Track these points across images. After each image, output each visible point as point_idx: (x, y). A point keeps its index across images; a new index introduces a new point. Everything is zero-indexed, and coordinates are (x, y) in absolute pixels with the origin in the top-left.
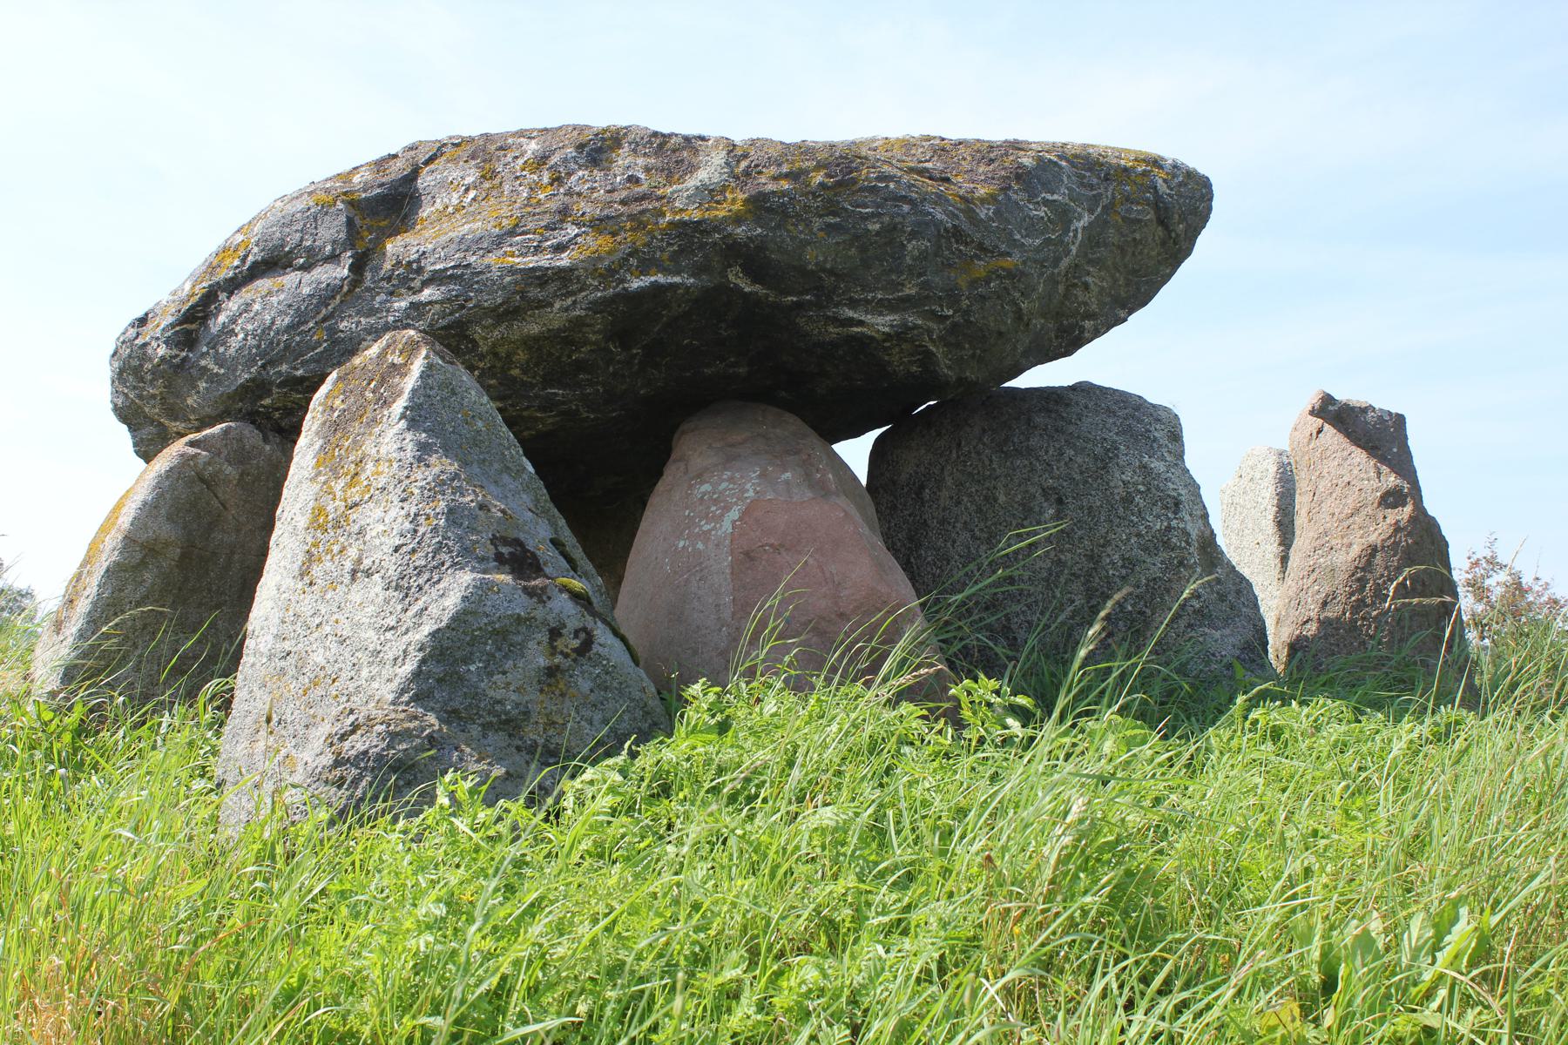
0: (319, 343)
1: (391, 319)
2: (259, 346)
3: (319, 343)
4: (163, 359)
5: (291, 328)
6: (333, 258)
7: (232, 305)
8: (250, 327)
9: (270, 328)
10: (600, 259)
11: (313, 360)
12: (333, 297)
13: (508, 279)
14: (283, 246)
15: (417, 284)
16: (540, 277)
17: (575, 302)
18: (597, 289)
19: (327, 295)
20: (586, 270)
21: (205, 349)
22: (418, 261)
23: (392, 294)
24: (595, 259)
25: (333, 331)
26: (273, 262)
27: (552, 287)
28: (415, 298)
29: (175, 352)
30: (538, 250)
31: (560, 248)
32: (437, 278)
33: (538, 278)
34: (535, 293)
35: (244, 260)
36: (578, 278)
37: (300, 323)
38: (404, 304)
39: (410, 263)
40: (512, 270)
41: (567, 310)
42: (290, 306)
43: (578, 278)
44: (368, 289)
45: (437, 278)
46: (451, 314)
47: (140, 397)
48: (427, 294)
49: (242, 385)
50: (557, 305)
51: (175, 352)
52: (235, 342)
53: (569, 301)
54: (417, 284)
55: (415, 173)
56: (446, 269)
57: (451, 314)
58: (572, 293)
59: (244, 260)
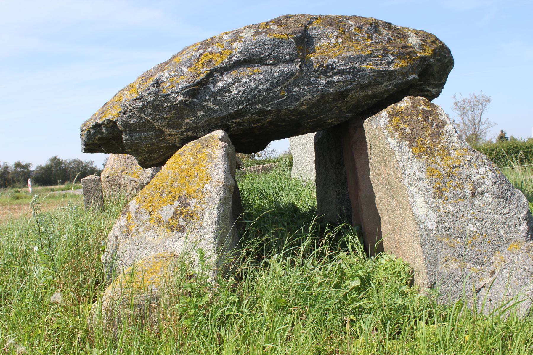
0: (283, 96)
1: (319, 87)
2: (246, 97)
3: (283, 96)
4: (181, 102)
5: (267, 90)
6: (290, 61)
7: (228, 78)
8: (242, 89)
9: (255, 90)
10: (404, 68)
11: (277, 103)
12: (291, 78)
13: (372, 74)
14: (260, 55)
15: (330, 74)
16: (382, 74)
17: (390, 84)
18: (400, 79)
19: (285, 77)
20: (399, 72)
21: (208, 98)
22: (332, 65)
23: (317, 77)
24: (402, 68)
25: (289, 91)
26: (249, 61)
27: (386, 78)
28: (330, 79)
29: (188, 98)
30: (381, 64)
31: (389, 63)
32: (341, 72)
33: (382, 74)
34: (380, 80)
35: (230, 59)
36: (395, 75)
37: (273, 88)
38: (324, 82)
39: (328, 66)
40: (374, 71)
41: (387, 86)
42: (267, 80)
43: (395, 75)
44: (306, 75)
45: (341, 72)
46: (345, 86)
47: (154, 119)
48: (336, 78)
49: (230, 114)
50: (384, 85)
51: (188, 98)
52: (228, 96)
53: (389, 83)
54: (330, 74)
55: (306, 29)
56: (346, 69)
57: (345, 86)
58: (391, 80)
59: (230, 59)
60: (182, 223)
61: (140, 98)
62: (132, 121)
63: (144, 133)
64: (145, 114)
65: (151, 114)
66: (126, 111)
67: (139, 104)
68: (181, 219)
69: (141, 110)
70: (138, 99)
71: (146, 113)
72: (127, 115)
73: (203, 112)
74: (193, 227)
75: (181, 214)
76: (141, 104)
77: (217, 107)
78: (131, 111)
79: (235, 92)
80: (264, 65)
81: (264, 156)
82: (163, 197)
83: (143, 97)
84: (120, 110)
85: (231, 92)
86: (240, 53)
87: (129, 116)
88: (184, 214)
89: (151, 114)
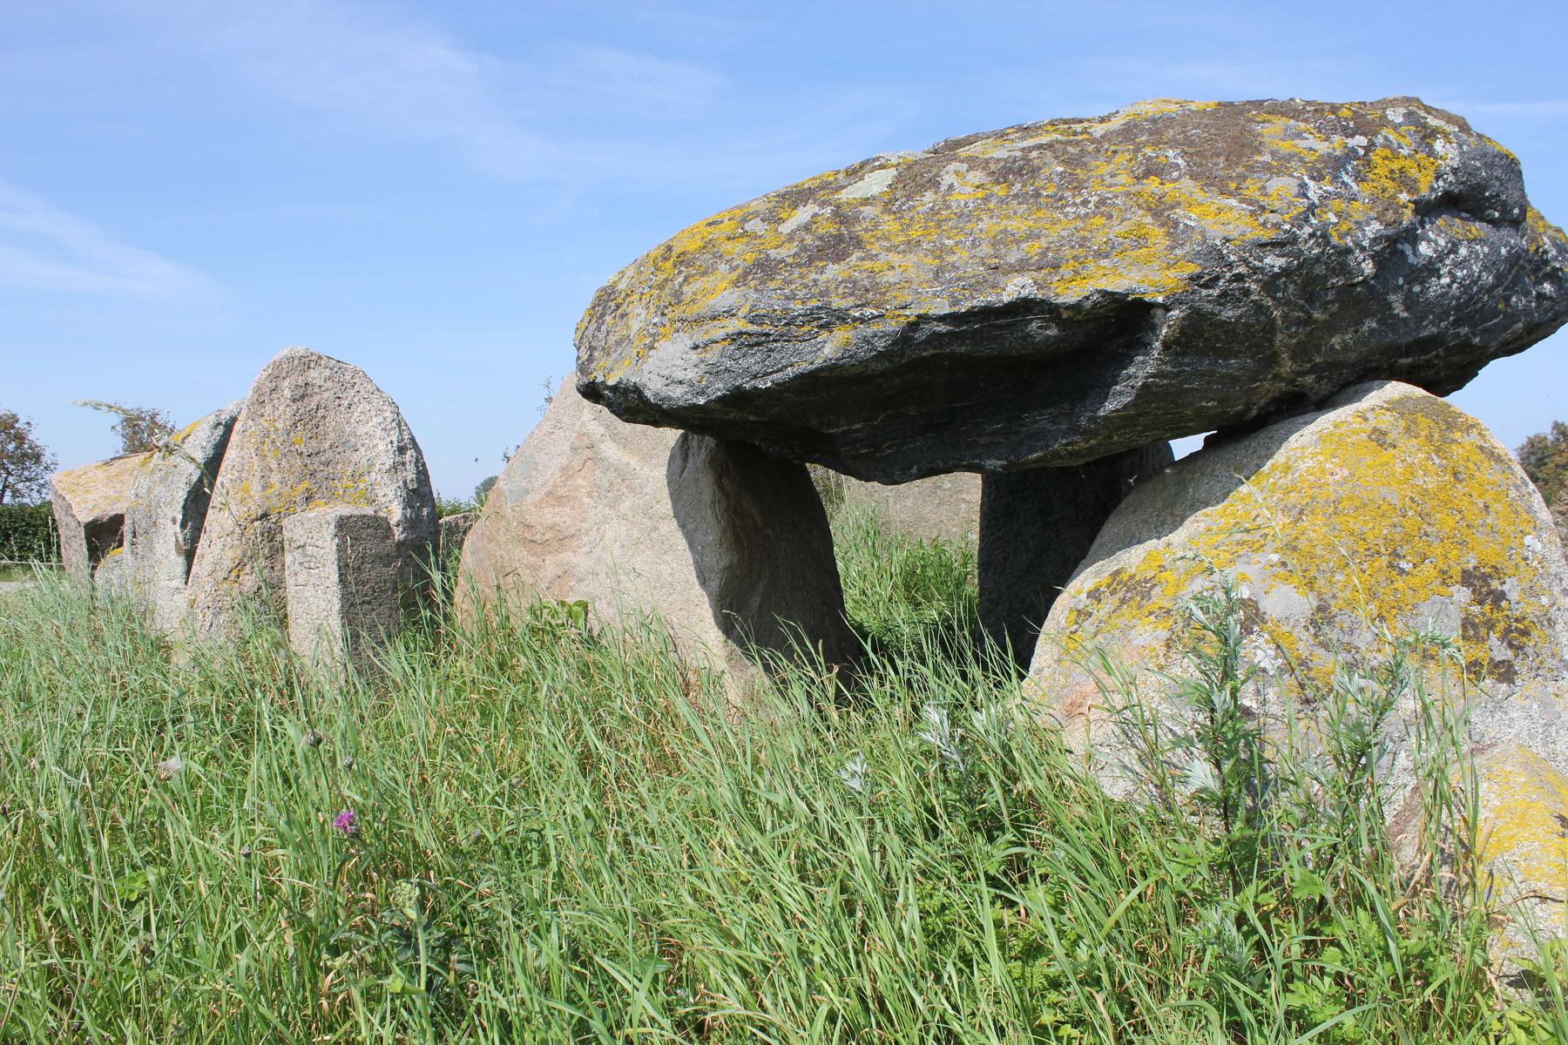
60: (1502, 653)
61: (1281, 244)
62: (1229, 314)
63: (1226, 358)
64: (1274, 298)
65: (1287, 303)
66: (1217, 278)
67: (1275, 262)
68: (1494, 638)
69: (1271, 283)
70: (1274, 244)
71: (1280, 295)
72: (1216, 292)
73: (1285, 317)
74: (1535, 665)
75: (1490, 625)
76: (1282, 262)
77: (1405, 315)
78: (1239, 278)
79: (1446, 280)
80: (1482, 220)
81: (35, 494)
82: (1402, 572)
83: (1294, 240)
84: (1193, 269)
85: (1439, 277)
86: (1455, 171)
87: (1224, 294)
88: (1501, 626)
89: (1287, 303)
